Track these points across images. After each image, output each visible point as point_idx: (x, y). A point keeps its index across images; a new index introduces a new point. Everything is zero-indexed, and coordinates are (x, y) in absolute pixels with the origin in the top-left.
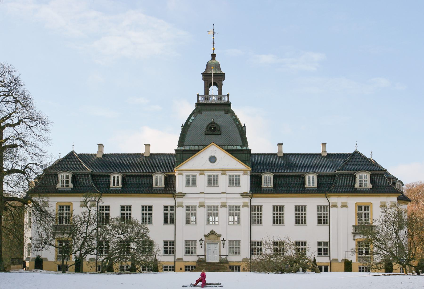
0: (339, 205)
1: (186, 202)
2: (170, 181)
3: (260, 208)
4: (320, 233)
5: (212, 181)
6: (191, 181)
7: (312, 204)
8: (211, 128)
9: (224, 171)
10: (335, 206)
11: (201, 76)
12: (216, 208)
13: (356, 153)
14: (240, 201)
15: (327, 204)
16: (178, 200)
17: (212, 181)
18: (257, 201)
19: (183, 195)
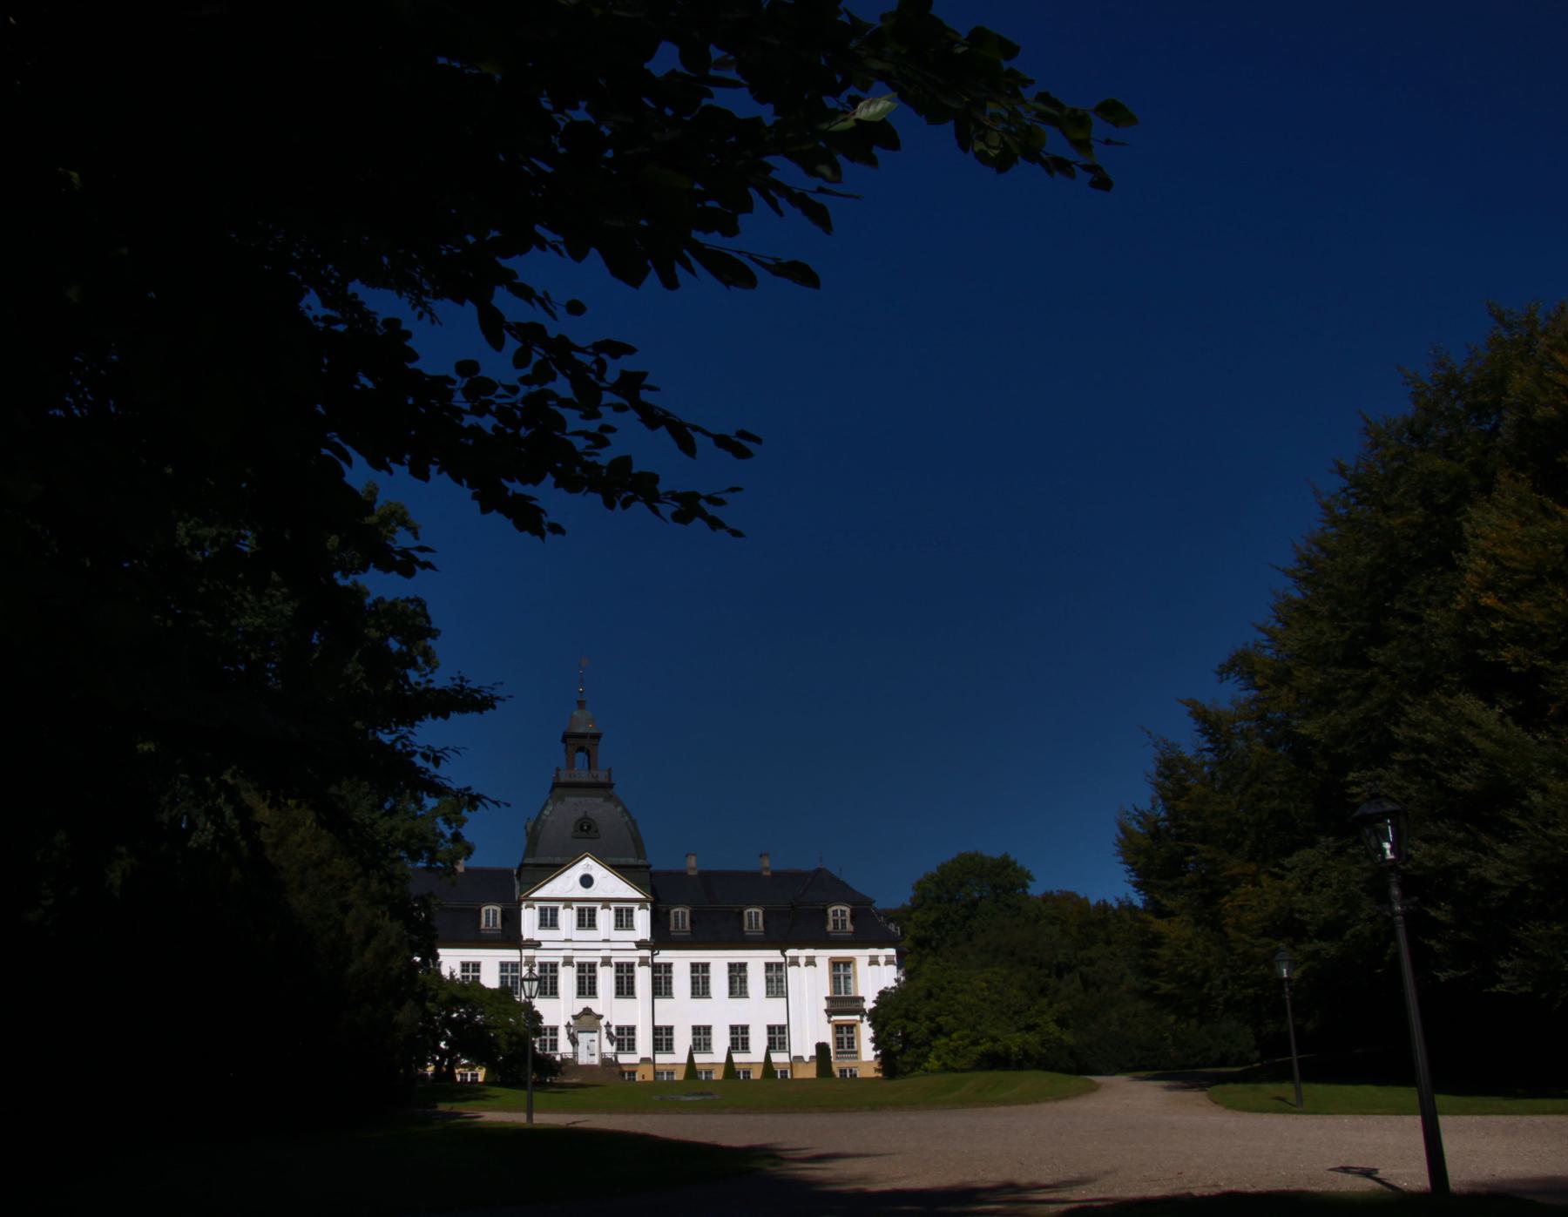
0: (802, 961)
1: (541, 956)
2: (512, 921)
3: (668, 967)
4: (774, 1012)
5: (586, 920)
6: (549, 920)
7: (756, 961)
9: (605, 902)
10: (795, 962)
12: (554, 966)
13: (819, 871)
14: (634, 956)
15: (782, 960)
17: (586, 920)
18: (664, 956)
19: (536, 945)
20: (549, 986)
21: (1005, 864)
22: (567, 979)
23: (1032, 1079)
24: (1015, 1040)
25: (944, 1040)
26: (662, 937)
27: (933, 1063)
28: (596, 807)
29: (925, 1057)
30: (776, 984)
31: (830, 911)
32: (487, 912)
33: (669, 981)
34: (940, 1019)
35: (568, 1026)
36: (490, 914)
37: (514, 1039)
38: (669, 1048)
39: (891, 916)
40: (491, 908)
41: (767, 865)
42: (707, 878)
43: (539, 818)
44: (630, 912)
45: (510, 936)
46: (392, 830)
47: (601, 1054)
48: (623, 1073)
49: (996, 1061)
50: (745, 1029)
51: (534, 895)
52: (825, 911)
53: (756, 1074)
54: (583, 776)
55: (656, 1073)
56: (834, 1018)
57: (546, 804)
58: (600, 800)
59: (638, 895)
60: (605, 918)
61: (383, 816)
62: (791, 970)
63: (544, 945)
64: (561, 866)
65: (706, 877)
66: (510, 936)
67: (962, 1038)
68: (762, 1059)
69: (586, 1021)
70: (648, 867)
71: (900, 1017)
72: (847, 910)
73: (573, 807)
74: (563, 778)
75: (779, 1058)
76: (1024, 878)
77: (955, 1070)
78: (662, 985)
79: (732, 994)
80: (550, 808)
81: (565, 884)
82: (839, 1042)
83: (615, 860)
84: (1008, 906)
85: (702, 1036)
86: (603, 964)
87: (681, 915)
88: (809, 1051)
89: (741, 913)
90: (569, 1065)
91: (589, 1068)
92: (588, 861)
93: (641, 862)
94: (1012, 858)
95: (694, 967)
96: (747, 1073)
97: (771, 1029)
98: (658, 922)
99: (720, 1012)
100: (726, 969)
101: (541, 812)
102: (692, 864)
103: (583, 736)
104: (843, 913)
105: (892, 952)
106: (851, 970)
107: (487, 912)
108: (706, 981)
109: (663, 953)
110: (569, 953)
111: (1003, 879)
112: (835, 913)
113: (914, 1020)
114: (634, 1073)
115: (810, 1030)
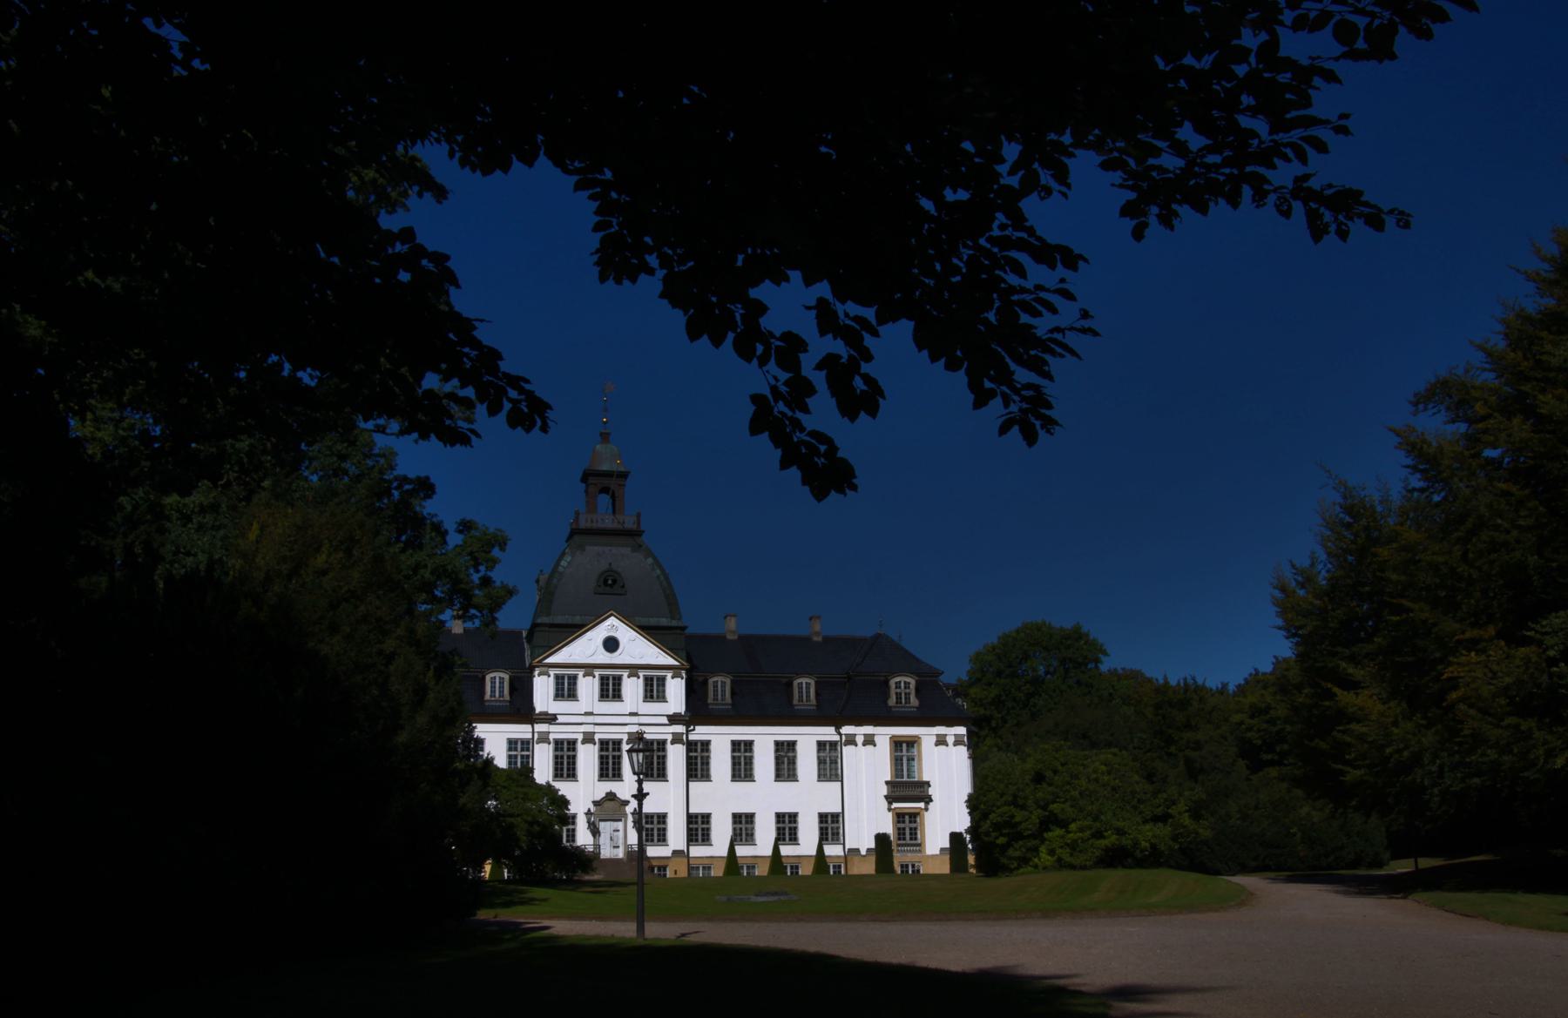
0: (860, 740)
1: (557, 732)
2: (522, 690)
3: (706, 745)
4: (825, 797)
5: (610, 690)
6: (566, 689)
7: (807, 739)
8: (606, 581)
9: (634, 669)
10: (851, 741)
11: (423, 475)
12: (572, 744)
13: (878, 636)
14: (666, 732)
15: (837, 738)
16: (540, 728)
17: (610, 690)
18: (701, 732)
19: (551, 719)
20: (565, 766)
21: (1077, 635)
22: (588, 758)
23: (1172, 882)
24: (1149, 835)
25: (1058, 832)
26: (699, 710)
27: (1045, 857)
28: (621, 557)
29: (1036, 850)
30: (830, 768)
31: (892, 683)
32: (493, 680)
33: (706, 762)
34: (1053, 807)
35: (588, 813)
36: (496, 683)
37: (537, 828)
38: (706, 839)
39: (960, 690)
40: (497, 675)
41: (818, 630)
42: (750, 644)
43: (554, 570)
44: (662, 680)
45: (520, 708)
46: (416, 568)
47: (626, 846)
48: (652, 868)
49: (1115, 858)
50: (793, 817)
51: (549, 660)
52: (886, 683)
53: (806, 870)
54: (608, 522)
55: (690, 868)
56: (895, 805)
57: (563, 554)
58: (627, 551)
59: (671, 661)
60: (632, 688)
61: (403, 551)
62: (847, 751)
63: (561, 719)
64: (580, 626)
65: (746, 641)
66: (520, 708)
67: (1081, 830)
68: (769, 852)
69: (609, 807)
70: (684, 628)
71: (1007, 804)
72: (912, 682)
73: (593, 559)
74: (583, 525)
75: (832, 850)
76: (1095, 651)
77: (1073, 867)
78: (698, 768)
79: (779, 777)
80: (568, 558)
81: (585, 648)
82: (900, 833)
83: (644, 621)
84: (1078, 682)
85: (743, 825)
86: (584, 742)
87: (720, 686)
88: (866, 843)
89: (790, 685)
90: (585, 860)
91: (614, 862)
92: (612, 621)
93: (674, 623)
94: (1085, 630)
95: (736, 745)
96: (795, 868)
97: (823, 817)
98: (694, 693)
99: (765, 797)
100: (772, 747)
101: (558, 564)
102: (731, 627)
103: (608, 474)
104: (907, 685)
105: (962, 730)
106: (915, 750)
107: (493, 680)
108: (749, 762)
109: (699, 729)
110: (589, 729)
111: (1073, 652)
112: (898, 685)
113: (1023, 807)
114: (665, 868)
115: (868, 819)
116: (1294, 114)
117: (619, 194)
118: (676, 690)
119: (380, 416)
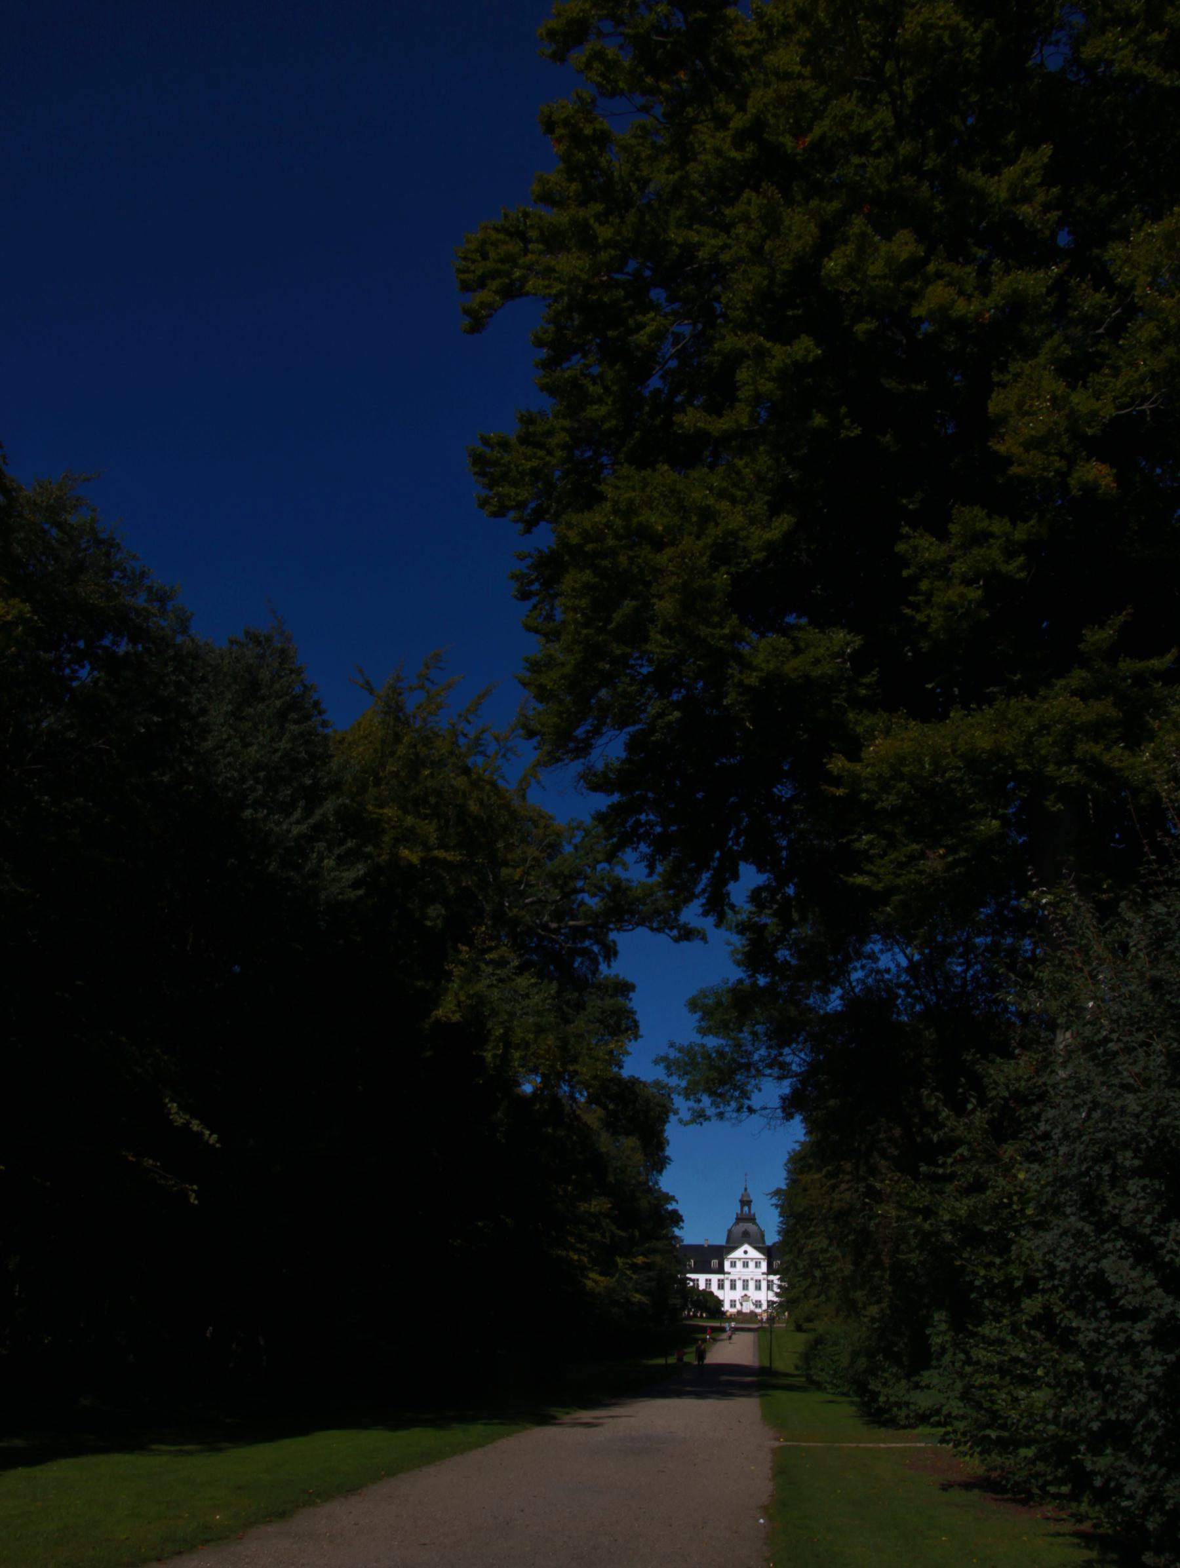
1: (731, 1277)
2: (721, 1265)
5: (746, 1265)
6: (733, 1265)
14: (761, 1277)
17: (746, 1265)
28: (750, 1227)
36: (715, 1263)
60: (752, 1264)
81: (738, 1253)
90: (724, 1313)
98: (769, 1265)
116: (725, 1378)
117: (718, 859)
118: (764, 1265)
119: (780, 1287)
